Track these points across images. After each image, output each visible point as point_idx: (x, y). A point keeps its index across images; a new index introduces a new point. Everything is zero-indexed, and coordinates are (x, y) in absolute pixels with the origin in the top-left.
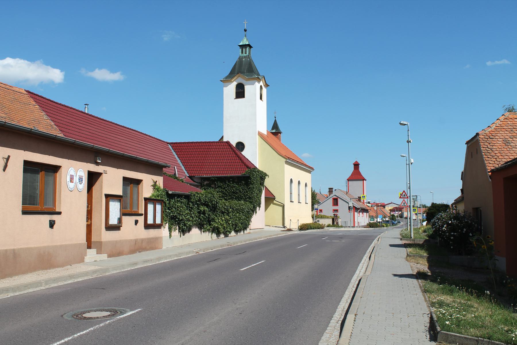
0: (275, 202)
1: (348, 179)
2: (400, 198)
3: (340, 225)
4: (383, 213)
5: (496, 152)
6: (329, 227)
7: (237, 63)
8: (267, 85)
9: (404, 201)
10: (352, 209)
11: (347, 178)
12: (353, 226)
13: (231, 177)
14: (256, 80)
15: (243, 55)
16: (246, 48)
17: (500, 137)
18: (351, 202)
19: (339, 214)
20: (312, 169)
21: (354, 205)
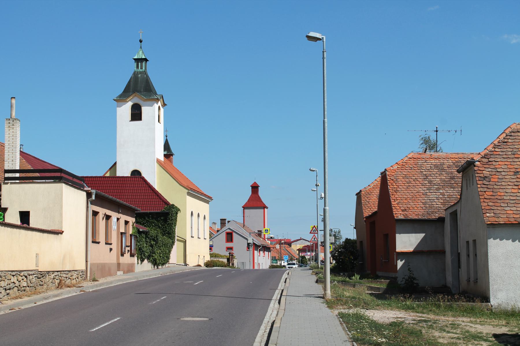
2: (310, 233)
4: (288, 253)
5: (371, 204)
7: (132, 80)
8: (164, 105)
9: (314, 237)
10: (251, 246)
11: (243, 204)
13: (150, 213)
14: (155, 101)
15: (138, 70)
16: (142, 62)
17: (375, 193)
18: (250, 237)
19: (235, 252)
20: (210, 198)
21: (254, 242)
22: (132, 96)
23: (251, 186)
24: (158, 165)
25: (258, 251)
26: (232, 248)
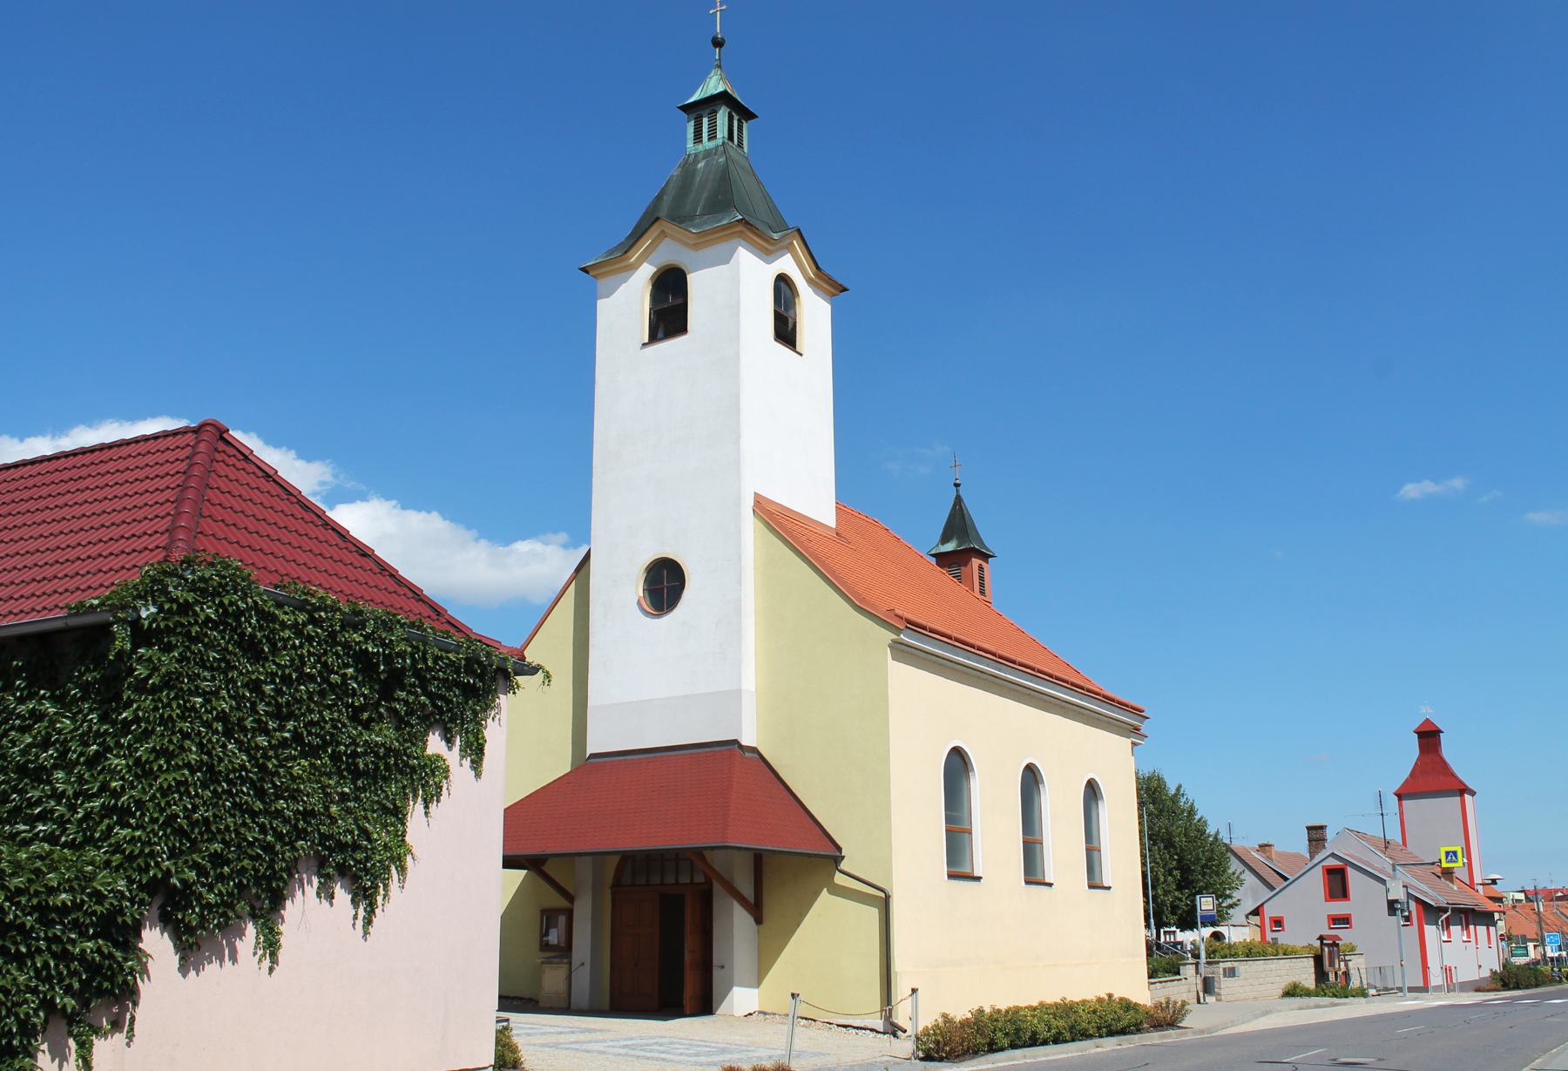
0: (839, 879)
1: (1398, 790)
3: (1355, 983)
6: (1293, 995)
11: (1397, 785)
14: (741, 234)
22: (645, 236)
23: (1415, 732)
24: (761, 525)
26: (1348, 919)
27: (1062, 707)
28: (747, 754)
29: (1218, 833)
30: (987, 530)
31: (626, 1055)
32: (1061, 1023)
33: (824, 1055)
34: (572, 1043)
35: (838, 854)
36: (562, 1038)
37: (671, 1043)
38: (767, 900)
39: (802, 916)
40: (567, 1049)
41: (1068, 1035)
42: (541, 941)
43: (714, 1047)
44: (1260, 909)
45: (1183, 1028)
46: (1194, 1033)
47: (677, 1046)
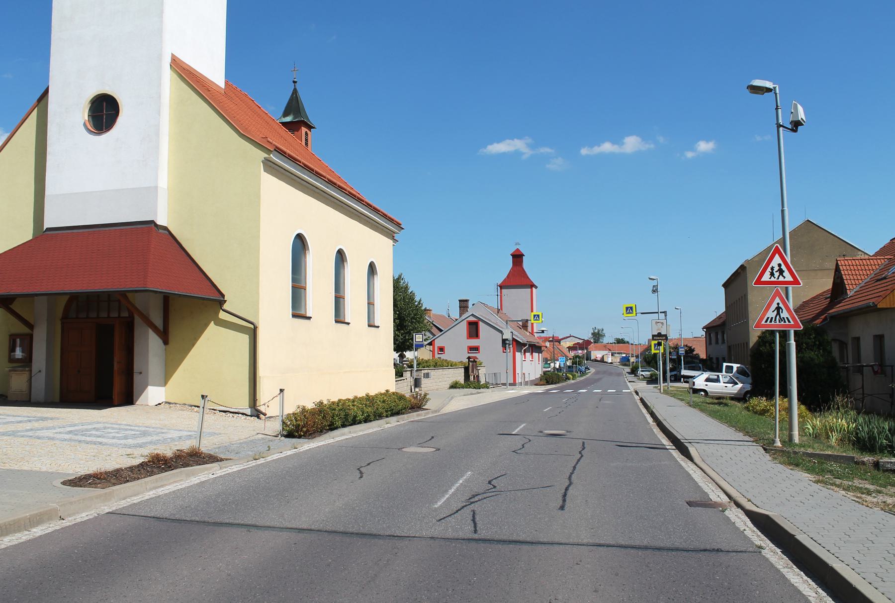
0: (222, 315)
3: (483, 381)
4: (562, 353)
6: (455, 388)
10: (509, 345)
11: (500, 282)
12: (512, 382)
18: (507, 328)
21: (514, 337)
24: (175, 76)
25: (523, 354)
26: (477, 348)
27: (359, 216)
28: (160, 231)
29: (420, 300)
30: (312, 113)
31: (70, 440)
32: (370, 409)
33: (217, 435)
34: (27, 430)
35: (222, 299)
36: (20, 427)
37: (105, 428)
38: (172, 329)
39: (196, 339)
40: (23, 436)
41: (372, 417)
42: (10, 356)
43: (137, 431)
44: (433, 342)
45: (427, 409)
46: (433, 412)
47: (110, 430)
